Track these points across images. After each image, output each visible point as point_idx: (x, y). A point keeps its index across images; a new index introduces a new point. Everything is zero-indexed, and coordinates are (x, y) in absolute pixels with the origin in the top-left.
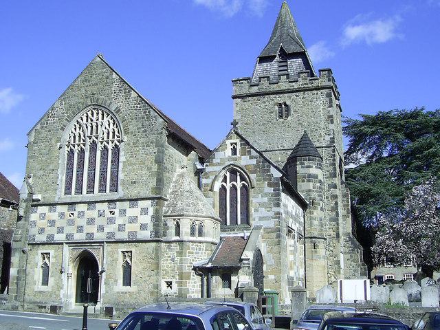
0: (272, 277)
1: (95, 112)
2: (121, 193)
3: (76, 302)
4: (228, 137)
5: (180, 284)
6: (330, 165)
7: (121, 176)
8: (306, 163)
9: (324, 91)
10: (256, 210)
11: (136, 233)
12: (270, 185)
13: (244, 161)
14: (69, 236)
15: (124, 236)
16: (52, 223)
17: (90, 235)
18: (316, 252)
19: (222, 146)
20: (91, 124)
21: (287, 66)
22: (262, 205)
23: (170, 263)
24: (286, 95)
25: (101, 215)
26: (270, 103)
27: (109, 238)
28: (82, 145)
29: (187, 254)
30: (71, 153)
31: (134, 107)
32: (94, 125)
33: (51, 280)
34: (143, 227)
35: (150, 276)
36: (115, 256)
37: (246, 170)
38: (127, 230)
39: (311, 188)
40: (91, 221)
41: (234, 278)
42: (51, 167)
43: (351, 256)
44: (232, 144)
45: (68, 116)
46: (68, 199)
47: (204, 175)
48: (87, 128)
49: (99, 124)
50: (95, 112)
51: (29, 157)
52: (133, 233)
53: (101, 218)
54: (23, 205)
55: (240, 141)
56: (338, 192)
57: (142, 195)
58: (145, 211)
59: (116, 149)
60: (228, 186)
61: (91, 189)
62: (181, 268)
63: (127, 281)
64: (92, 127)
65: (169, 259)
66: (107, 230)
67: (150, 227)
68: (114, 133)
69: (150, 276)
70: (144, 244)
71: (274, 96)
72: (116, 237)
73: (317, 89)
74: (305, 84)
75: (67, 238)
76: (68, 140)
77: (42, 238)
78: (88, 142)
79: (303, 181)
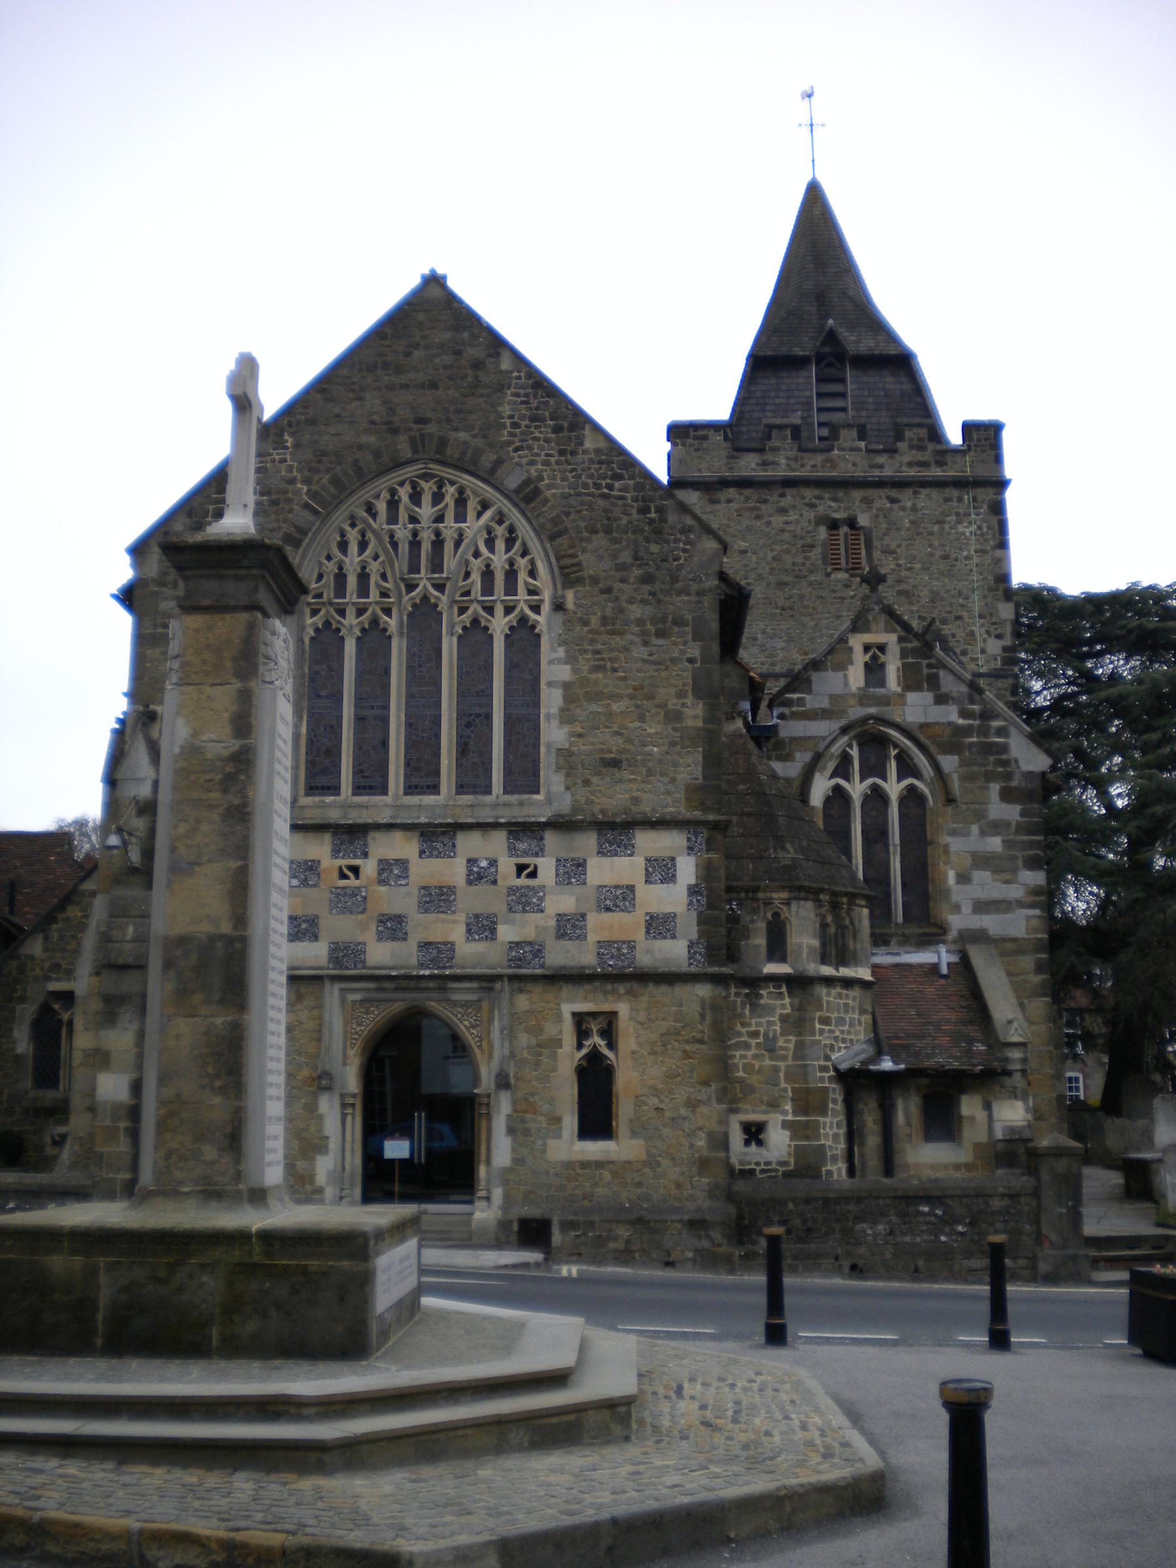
1: (428, 487)
2: (554, 794)
4: (859, 624)
7: (553, 734)
12: (1007, 795)
14: (344, 953)
15: (584, 956)
20: (415, 534)
21: (843, 395)
22: (984, 861)
23: (755, 1057)
24: (857, 494)
25: (478, 875)
27: (519, 961)
29: (818, 1026)
32: (427, 537)
34: (659, 925)
35: (692, 1104)
36: (550, 1029)
37: (926, 742)
38: (592, 937)
40: (438, 898)
44: (867, 648)
50: (428, 487)
53: (483, 888)
55: (901, 640)
57: (649, 806)
60: (857, 789)
61: (422, 778)
63: (596, 1119)
65: (753, 1042)
66: (506, 933)
67: (688, 927)
70: (664, 988)
71: (817, 492)
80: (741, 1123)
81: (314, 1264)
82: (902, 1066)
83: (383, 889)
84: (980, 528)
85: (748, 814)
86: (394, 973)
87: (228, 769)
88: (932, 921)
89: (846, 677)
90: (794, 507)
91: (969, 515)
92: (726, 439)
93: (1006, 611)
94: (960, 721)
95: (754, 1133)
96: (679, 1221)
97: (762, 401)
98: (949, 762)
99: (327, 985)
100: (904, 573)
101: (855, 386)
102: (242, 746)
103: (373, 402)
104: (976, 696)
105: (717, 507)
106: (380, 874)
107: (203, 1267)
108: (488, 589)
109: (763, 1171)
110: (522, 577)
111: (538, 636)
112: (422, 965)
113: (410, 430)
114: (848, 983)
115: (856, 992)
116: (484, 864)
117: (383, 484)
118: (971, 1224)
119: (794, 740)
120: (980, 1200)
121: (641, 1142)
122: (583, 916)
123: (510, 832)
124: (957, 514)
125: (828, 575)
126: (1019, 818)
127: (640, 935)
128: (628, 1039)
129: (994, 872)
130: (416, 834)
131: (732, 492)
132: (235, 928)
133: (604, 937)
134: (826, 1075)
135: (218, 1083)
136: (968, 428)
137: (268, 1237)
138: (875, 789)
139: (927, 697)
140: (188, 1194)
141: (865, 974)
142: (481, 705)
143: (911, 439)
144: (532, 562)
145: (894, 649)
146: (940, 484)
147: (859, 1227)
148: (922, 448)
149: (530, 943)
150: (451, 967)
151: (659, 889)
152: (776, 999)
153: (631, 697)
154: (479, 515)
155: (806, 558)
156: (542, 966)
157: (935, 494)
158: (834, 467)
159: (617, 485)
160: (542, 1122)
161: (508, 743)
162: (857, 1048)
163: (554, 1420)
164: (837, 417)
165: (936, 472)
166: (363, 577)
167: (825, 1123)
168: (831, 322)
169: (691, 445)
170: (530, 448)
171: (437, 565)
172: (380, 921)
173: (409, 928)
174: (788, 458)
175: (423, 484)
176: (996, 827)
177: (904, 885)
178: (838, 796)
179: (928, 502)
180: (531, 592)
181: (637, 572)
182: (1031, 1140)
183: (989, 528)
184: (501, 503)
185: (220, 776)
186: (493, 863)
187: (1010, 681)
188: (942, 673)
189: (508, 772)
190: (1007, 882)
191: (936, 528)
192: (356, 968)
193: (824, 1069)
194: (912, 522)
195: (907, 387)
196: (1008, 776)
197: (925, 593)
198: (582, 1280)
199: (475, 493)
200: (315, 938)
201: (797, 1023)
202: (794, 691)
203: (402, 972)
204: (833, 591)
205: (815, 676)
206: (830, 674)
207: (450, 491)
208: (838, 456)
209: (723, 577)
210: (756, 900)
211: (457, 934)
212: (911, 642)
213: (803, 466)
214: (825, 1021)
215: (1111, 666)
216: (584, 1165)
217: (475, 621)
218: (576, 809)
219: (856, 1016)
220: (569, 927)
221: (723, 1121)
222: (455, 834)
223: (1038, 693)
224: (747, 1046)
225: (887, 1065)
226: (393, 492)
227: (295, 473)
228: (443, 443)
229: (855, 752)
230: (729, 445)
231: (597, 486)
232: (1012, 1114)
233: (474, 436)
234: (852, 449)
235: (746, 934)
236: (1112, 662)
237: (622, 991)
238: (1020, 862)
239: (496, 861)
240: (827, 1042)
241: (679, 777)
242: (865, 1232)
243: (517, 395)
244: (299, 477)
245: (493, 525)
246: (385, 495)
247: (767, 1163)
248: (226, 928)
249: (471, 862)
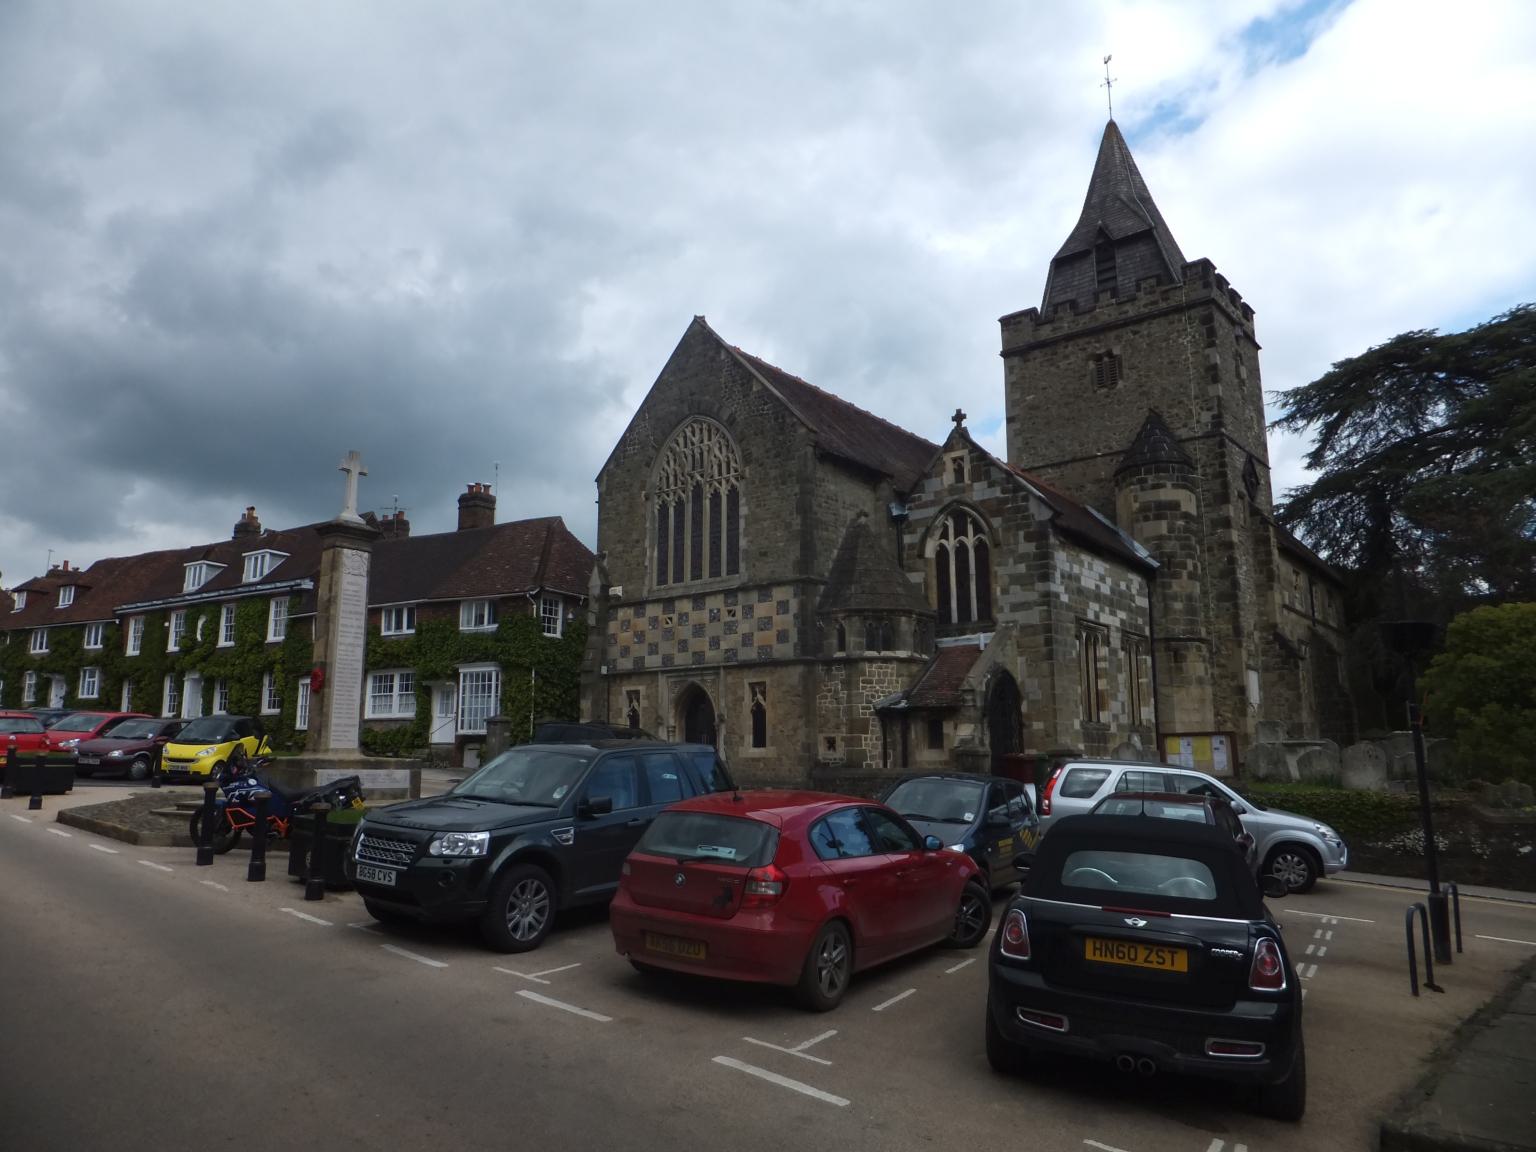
0: (1038, 726)
2: (743, 576)
5: (849, 742)
6: (1215, 476)
7: (743, 543)
8: (1151, 479)
9: (1193, 313)
12: (1028, 538)
15: (750, 654)
18: (1180, 669)
22: (1016, 579)
23: (830, 703)
24: (1112, 335)
25: (714, 618)
26: (1074, 357)
28: (680, 492)
36: (740, 693)
39: (1164, 531)
40: (699, 630)
42: (635, 536)
43: (1282, 677)
47: (907, 527)
48: (686, 458)
49: (705, 449)
51: (1278, 392)
53: (715, 624)
54: (594, 606)
55: (970, 452)
56: (1235, 536)
59: (733, 494)
60: (951, 544)
61: (697, 574)
62: (849, 711)
63: (760, 741)
64: (693, 456)
65: (829, 694)
66: (724, 645)
67: (794, 637)
68: (728, 464)
71: (1087, 339)
72: (739, 658)
73: (1179, 309)
75: (663, 663)
77: (625, 664)
79: (1146, 519)
80: (826, 738)
84: (1194, 337)
89: (942, 480)
90: (1073, 353)
91: (1186, 330)
92: (1031, 320)
94: (1002, 496)
95: (831, 744)
98: (996, 522)
99: (660, 676)
105: (1028, 363)
112: (693, 664)
114: (886, 660)
119: (917, 521)
124: (1178, 331)
125: (1095, 392)
127: (706, 648)
129: (1022, 585)
131: (1037, 353)
133: (760, 644)
134: (868, 711)
139: (984, 484)
143: (1145, 288)
145: (967, 459)
146: (1164, 314)
153: (771, 518)
155: (1082, 384)
156: (737, 661)
157: (1162, 320)
159: (766, 407)
160: (738, 739)
161: (728, 550)
174: (1068, 323)
176: (1021, 558)
178: (942, 553)
179: (1157, 328)
181: (774, 452)
183: (1200, 335)
186: (719, 610)
187: (1218, 439)
191: (1164, 344)
193: (868, 708)
194: (1148, 344)
197: (1157, 391)
200: (657, 653)
201: (848, 684)
204: (1099, 402)
206: (934, 479)
213: (1077, 325)
216: (753, 760)
218: (750, 580)
219: (894, 678)
220: (747, 640)
224: (826, 697)
230: (1033, 323)
231: (758, 411)
232: (966, 731)
234: (1107, 306)
238: (1035, 578)
240: (870, 693)
248: (323, 660)
249: (711, 611)
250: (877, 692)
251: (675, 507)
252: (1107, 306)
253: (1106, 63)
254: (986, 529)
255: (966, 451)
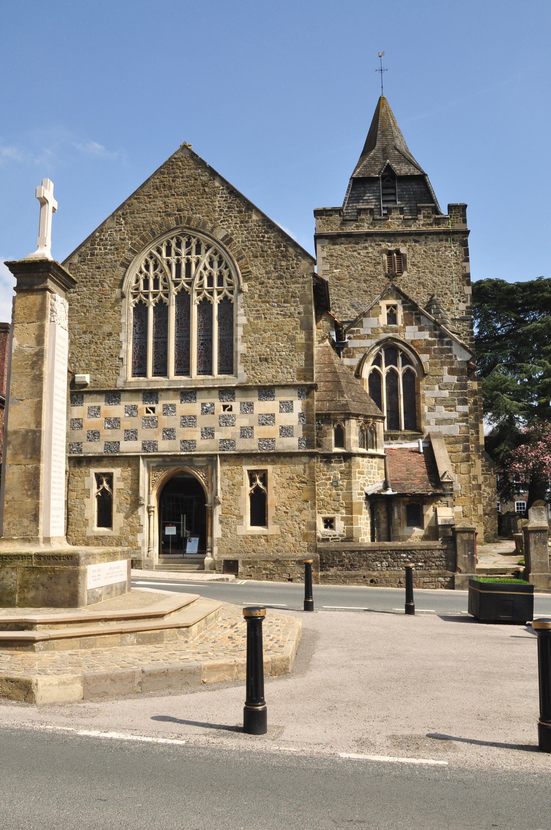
1: (184, 240)
2: (242, 375)
3: (159, 553)
7: (241, 347)
10: (431, 410)
11: (273, 441)
12: (451, 372)
13: (411, 334)
14: (149, 445)
16: (114, 423)
17: (188, 444)
19: (373, 311)
20: (178, 260)
21: (394, 194)
22: (439, 401)
23: (330, 489)
25: (206, 411)
26: (372, 250)
29: (357, 475)
30: (140, 311)
31: (258, 236)
33: (118, 518)
34: (286, 431)
36: (238, 478)
38: (256, 437)
40: (189, 421)
41: (429, 512)
42: (107, 328)
44: (388, 307)
45: (133, 245)
46: (141, 383)
50: (184, 240)
52: (267, 441)
53: (209, 416)
55: (403, 303)
58: (287, 407)
60: (384, 371)
61: (183, 368)
63: (259, 516)
65: (328, 482)
66: (218, 436)
67: (299, 432)
69: (300, 511)
71: (381, 239)
74: (428, 224)
75: (144, 448)
76: (134, 285)
78: (174, 291)
81: (57, 567)
82: (396, 493)
83: (165, 417)
85: (328, 382)
86: (170, 454)
87: (34, 359)
88: (417, 428)
93: (468, 290)
95: (329, 523)
96: (294, 561)
97: (357, 198)
100: (421, 274)
101: (400, 190)
102: (40, 349)
103: (159, 203)
104: (437, 327)
106: (163, 411)
107: (13, 568)
108: (210, 283)
109: (332, 539)
110: (226, 278)
111: (233, 304)
112: (182, 450)
113: (175, 214)
114: (372, 456)
115: (377, 460)
116: (209, 405)
117: (163, 240)
118: (425, 562)
120: (429, 551)
121: (278, 526)
122: (252, 428)
123: (220, 391)
124: (445, 247)
126: (456, 382)
127: (277, 436)
128: (271, 483)
129: (445, 407)
130: (179, 392)
132: (37, 427)
134: (362, 497)
135: (29, 493)
136: (451, 208)
137: (39, 556)
138: (392, 370)
140: (16, 539)
141: (381, 452)
142: (208, 336)
144: (230, 272)
147: (375, 563)
148: (429, 217)
149: (229, 440)
150: (194, 451)
151: (285, 415)
152: (338, 463)
154: (206, 251)
158: (389, 227)
162: (376, 485)
163: (149, 632)
164: (390, 205)
165: (435, 228)
166: (156, 281)
167: (360, 518)
168: (388, 161)
169: (324, 219)
170: (228, 221)
171: (188, 274)
172: (164, 431)
173: (176, 434)
175: (181, 238)
176: (446, 386)
177: (405, 413)
180: (229, 285)
182: (454, 525)
183: (460, 253)
184: (216, 246)
185: (31, 362)
186: (213, 405)
188: (422, 317)
189: (220, 364)
190: (451, 411)
192: (154, 451)
193: (361, 494)
195: (423, 190)
196: (452, 363)
198: (245, 586)
199: (205, 242)
202: (355, 327)
203: (173, 453)
205: (365, 320)
207: (194, 241)
208: (391, 222)
209: (314, 275)
210: (330, 419)
211: (197, 436)
212: (408, 303)
214: (361, 473)
215: (532, 316)
216: (253, 537)
217: (205, 298)
219: (377, 471)
220: (246, 432)
221: (314, 517)
222: (196, 393)
223: (499, 329)
225: (390, 492)
226: (169, 242)
227: (126, 236)
228: (189, 220)
229: (383, 354)
231: (258, 236)
233: (203, 216)
234: (397, 219)
235: (325, 435)
236: (533, 315)
237: (269, 460)
238: (456, 402)
239: (214, 404)
241: (294, 365)
242: (377, 565)
243: (221, 197)
244: (127, 237)
245: (212, 255)
246: (165, 244)
247: (335, 535)
248: (33, 427)
249: (203, 404)
250: (366, 481)
251: (154, 308)
252: (397, 219)
253: (380, 56)
254: (415, 362)
255: (400, 301)
